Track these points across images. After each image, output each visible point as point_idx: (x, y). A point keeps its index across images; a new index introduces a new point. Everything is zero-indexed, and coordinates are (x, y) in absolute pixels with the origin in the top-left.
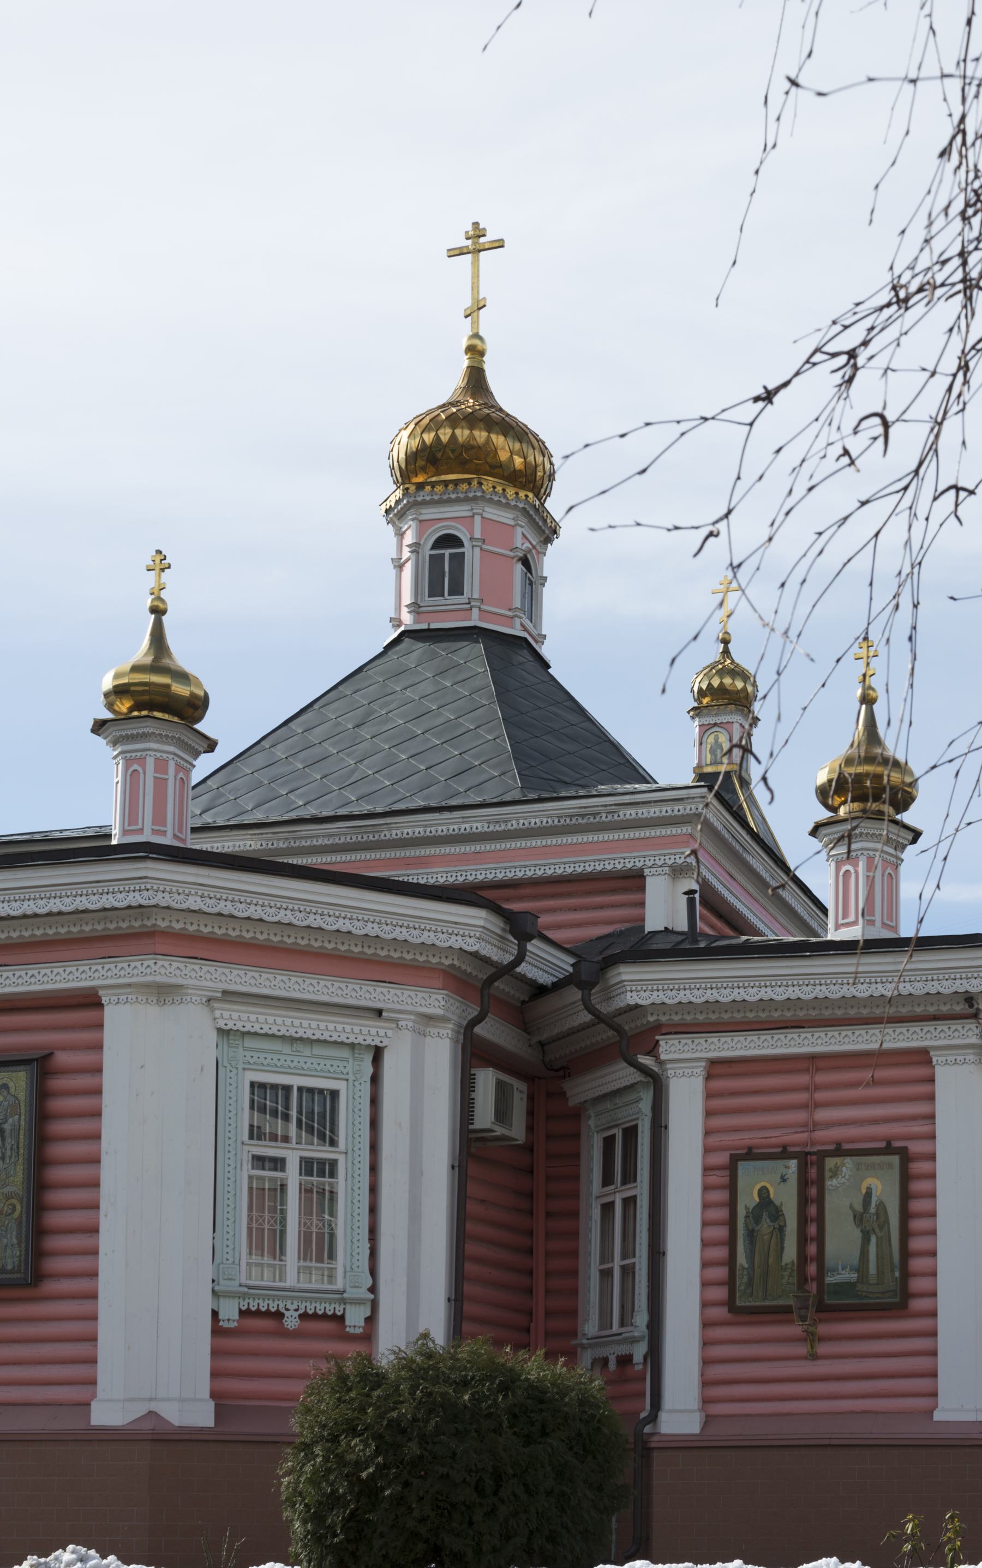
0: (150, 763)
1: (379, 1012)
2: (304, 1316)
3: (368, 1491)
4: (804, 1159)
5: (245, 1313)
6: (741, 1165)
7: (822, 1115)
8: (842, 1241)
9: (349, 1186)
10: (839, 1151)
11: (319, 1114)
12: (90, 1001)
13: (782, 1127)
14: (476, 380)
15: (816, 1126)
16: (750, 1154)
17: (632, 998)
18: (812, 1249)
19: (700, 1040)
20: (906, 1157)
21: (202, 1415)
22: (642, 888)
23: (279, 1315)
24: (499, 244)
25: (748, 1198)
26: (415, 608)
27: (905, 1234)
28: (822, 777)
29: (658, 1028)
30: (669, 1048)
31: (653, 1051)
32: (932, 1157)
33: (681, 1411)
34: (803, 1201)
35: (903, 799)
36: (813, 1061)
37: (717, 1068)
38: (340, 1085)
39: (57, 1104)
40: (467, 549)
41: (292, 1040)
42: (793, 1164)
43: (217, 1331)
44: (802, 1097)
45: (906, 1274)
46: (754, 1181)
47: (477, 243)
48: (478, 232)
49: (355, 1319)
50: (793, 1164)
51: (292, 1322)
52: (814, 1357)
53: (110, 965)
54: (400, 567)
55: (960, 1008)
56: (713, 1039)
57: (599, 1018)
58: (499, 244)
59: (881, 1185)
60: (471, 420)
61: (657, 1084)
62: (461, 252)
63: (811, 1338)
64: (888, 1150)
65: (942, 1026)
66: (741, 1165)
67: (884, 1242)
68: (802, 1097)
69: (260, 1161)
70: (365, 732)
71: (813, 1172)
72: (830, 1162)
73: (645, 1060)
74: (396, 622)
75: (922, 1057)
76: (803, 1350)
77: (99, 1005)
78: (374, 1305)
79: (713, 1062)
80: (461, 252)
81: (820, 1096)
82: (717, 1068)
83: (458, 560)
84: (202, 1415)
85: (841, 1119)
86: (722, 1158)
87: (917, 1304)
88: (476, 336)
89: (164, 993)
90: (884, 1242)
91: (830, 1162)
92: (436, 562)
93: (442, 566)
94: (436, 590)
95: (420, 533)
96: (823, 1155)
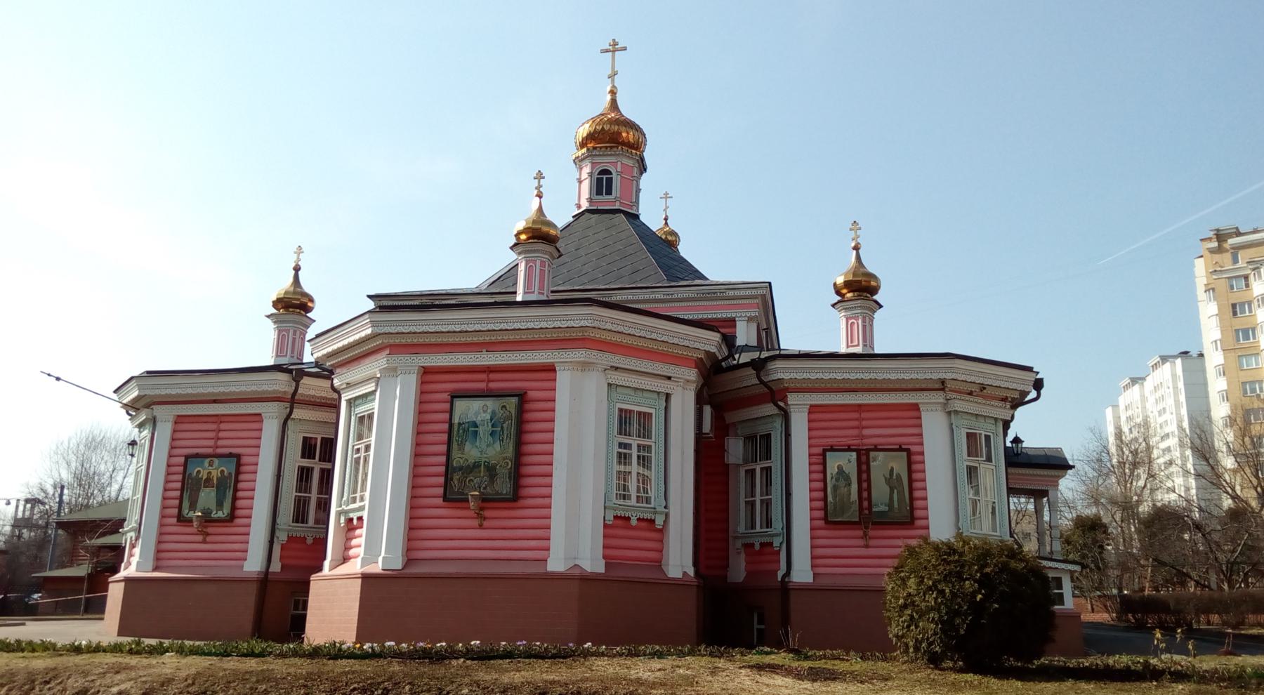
0: (538, 263)
1: (669, 378)
2: (639, 519)
3: (978, 609)
4: (858, 451)
5: (616, 517)
6: (828, 454)
7: (866, 432)
8: (880, 491)
9: (656, 457)
10: (876, 449)
11: (645, 417)
12: (551, 369)
13: (846, 435)
14: (614, 105)
15: (863, 437)
16: (832, 449)
17: (780, 376)
18: (865, 494)
19: (807, 395)
20: (908, 450)
21: (600, 567)
22: (735, 326)
23: (629, 519)
24: (625, 49)
25: (832, 469)
26: (590, 200)
27: (911, 490)
28: (840, 280)
29: (788, 390)
30: (792, 399)
31: (784, 399)
32: (922, 453)
33: (802, 573)
34: (860, 472)
35: (874, 290)
36: (859, 408)
37: (813, 409)
38: (652, 411)
39: (529, 416)
40: (614, 176)
41: (636, 389)
42: (854, 454)
43: (606, 526)
44: (856, 423)
45: (912, 509)
46: (835, 462)
47: (614, 48)
48: (615, 43)
49: (659, 521)
50: (854, 454)
51: (634, 522)
52: (867, 546)
53: (562, 352)
54: (580, 182)
55: (937, 386)
56: (814, 395)
57: (762, 382)
58: (625, 49)
59: (898, 464)
60: (611, 121)
61: (786, 416)
62: (607, 51)
63: (865, 536)
64: (900, 449)
65: (926, 393)
66: (828, 454)
67: (901, 493)
68: (856, 423)
69: (621, 445)
70: (581, 252)
71: (864, 458)
72: (872, 454)
73: (781, 404)
74: (579, 206)
75: (915, 407)
76: (861, 542)
77: (554, 370)
78: (667, 515)
79: (811, 406)
80: (607, 51)
81: (864, 423)
82: (813, 409)
83: (610, 181)
84: (600, 567)
85: (874, 434)
86: (819, 450)
87: (918, 523)
88: (614, 86)
89: (585, 366)
90: (901, 493)
91: (872, 454)
92: (599, 181)
93: (602, 184)
94: (599, 192)
95: (592, 168)
96: (868, 451)
